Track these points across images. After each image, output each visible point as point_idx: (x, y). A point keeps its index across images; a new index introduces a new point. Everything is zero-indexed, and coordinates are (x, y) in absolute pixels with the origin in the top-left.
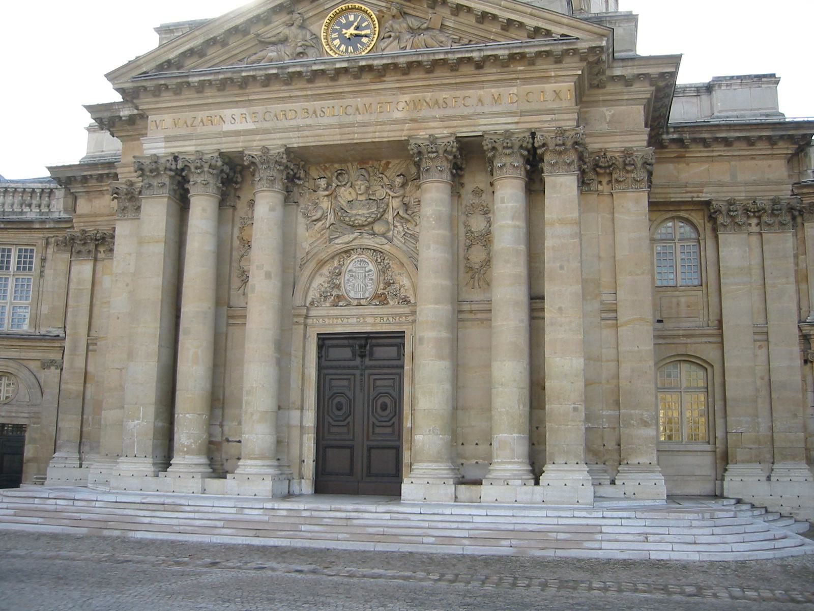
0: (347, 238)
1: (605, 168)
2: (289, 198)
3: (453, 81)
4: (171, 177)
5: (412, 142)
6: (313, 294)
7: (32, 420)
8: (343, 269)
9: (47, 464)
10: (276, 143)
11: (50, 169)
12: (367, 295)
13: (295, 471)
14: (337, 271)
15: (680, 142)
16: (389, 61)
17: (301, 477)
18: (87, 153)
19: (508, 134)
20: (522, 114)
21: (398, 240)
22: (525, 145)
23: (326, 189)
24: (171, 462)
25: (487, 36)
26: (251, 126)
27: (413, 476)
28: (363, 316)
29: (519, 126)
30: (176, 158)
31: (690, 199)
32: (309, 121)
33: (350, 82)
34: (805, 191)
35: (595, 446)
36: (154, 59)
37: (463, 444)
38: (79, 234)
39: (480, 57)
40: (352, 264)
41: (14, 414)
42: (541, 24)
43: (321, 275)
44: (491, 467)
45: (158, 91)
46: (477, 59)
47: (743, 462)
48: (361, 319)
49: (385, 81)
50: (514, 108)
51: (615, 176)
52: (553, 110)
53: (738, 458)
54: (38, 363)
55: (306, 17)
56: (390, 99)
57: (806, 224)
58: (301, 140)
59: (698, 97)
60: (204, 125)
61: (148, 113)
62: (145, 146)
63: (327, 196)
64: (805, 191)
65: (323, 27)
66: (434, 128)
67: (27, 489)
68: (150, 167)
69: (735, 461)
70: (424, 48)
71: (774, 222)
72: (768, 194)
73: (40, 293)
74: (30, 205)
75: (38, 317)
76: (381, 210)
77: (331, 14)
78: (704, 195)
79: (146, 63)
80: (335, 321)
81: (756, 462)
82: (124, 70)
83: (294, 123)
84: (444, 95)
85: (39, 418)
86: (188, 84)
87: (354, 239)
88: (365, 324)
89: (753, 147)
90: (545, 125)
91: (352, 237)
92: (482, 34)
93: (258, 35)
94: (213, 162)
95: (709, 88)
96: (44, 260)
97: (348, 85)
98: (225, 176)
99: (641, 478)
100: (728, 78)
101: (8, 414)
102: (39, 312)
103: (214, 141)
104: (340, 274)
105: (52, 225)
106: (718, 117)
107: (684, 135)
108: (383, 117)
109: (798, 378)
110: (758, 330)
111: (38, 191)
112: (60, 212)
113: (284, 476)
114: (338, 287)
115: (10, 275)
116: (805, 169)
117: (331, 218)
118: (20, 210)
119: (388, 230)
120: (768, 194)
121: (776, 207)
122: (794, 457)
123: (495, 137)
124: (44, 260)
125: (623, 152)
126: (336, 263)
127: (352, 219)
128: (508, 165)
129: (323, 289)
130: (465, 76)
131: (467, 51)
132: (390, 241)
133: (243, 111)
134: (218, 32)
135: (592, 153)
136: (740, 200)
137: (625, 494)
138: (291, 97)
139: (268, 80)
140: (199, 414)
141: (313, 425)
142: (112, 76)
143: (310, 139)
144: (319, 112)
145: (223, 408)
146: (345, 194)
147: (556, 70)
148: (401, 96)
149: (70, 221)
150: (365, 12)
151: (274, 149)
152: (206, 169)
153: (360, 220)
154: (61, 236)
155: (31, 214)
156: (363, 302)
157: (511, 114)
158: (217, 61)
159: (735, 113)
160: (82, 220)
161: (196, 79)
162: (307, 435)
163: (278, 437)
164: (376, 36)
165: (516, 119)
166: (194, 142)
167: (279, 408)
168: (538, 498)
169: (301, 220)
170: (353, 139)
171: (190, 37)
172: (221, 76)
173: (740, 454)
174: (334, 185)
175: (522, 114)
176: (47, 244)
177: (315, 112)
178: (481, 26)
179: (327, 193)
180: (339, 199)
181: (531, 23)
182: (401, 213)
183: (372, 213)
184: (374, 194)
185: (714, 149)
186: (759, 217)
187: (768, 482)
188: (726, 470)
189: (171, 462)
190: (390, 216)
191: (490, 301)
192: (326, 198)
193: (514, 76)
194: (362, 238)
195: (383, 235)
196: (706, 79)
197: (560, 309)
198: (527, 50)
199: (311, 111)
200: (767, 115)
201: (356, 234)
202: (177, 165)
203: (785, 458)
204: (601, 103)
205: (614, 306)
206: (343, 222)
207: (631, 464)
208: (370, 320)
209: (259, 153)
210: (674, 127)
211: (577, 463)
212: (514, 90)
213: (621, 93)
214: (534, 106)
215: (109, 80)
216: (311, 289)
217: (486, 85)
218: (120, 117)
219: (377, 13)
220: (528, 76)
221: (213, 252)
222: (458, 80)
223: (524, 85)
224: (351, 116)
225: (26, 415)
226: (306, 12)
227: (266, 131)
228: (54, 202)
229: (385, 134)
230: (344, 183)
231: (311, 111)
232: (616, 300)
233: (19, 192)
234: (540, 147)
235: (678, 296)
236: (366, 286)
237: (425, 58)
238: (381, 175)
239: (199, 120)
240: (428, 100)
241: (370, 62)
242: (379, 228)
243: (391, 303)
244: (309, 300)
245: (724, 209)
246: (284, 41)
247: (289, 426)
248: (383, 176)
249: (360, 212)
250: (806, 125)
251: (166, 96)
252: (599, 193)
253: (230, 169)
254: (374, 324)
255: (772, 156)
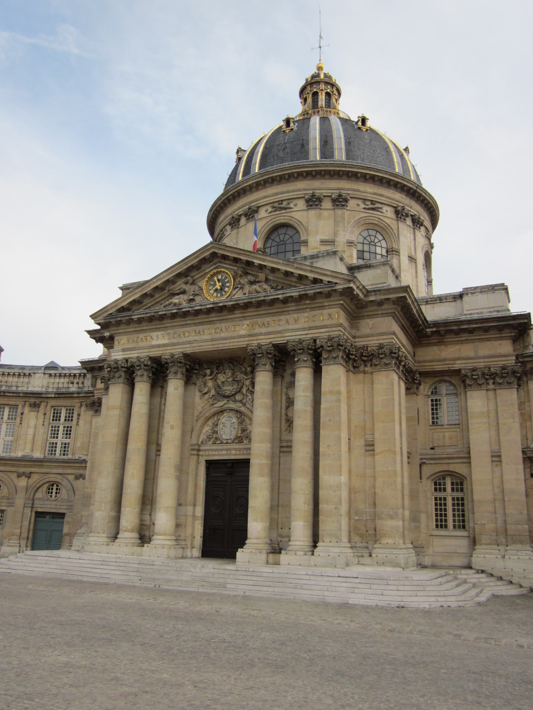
0: (221, 404)
1: (368, 357)
2: (188, 381)
3: (272, 311)
4: (125, 372)
5: (249, 348)
6: (203, 437)
7: (68, 510)
8: (220, 421)
9: (74, 536)
10: (178, 351)
11: (81, 362)
12: (232, 437)
13: (189, 543)
14: (216, 423)
15: (437, 333)
16: (235, 303)
17: (193, 547)
18: (103, 352)
19: (300, 342)
20: (310, 328)
21: (249, 404)
22: (310, 347)
23: (210, 375)
24: (118, 536)
25: (291, 283)
26: (166, 341)
27: (247, 547)
28: (230, 450)
29: (306, 336)
30: (127, 360)
31: (448, 369)
32: (197, 338)
33: (216, 315)
34: (527, 359)
35: (361, 531)
36: (115, 306)
37: (282, 528)
38: (97, 400)
39: (283, 297)
40: (224, 419)
41: (58, 507)
42: (316, 276)
43: (208, 425)
44: (291, 543)
45: (119, 323)
46: (281, 299)
47: (486, 544)
48: (229, 451)
49: (235, 313)
50: (306, 325)
51: (374, 361)
52: (326, 325)
53: (483, 542)
54: (73, 476)
55: (195, 278)
56: (238, 323)
57: (529, 382)
58: (191, 349)
59: (456, 302)
60: (142, 341)
61: (114, 335)
62: (112, 354)
63: (211, 379)
64: (527, 359)
65: (205, 283)
66: (261, 339)
67: (62, 553)
68: (114, 366)
69: (480, 543)
70: (255, 293)
71: (503, 382)
72: (499, 363)
73: (76, 434)
74: (73, 383)
75: (75, 448)
76: (239, 387)
77: (209, 276)
78: (457, 366)
79: (111, 308)
80: (215, 453)
81: (495, 544)
82: (100, 313)
83: (188, 339)
84: (268, 319)
85: (72, 509)
86: (132, 319)
87: (224, 404)
88: (230, 454)
89: (488, 333)
90: (322, 335)
91: (223, 403)
92: (288, 283)
93: (169, 290)
94: (146, 363)
95: (461, 296)
96: (79, 415)
97: (216, 317)
98: (154, 370)
99: (387, 552)
100: (473, 289)
101: (56, 507)
102: (75, 446)
103: (146, 350)
104: (217, 425)
105: (83, 395)
106: (465, 315)
107: (440, 328)
108: (235, 334)
109: (522, 488)
110: (495, 454)
111: (77, 375)
112: (89, 387)
113: (179, 546)
114: (217, 432)
115: (60, 424)
116: (528, 344)
117: (213, 392)
118: (67, 386)
119: (243, 399)
120: (499, 363)
121: (503, 371)
122: (521, 542)
123: (294, 344)
124: (79, 415)
125: (378, 346)
126: (216, 418)
127: (223, 392)
128: (301, 359)
129: (208, 434)
130: (278, 308)
131: (276, 295)
132: (244, 405)
133: (163, 333)
134: (148, 289)
135: (360, 348)
136: (480, 368)
137: (377, 563)
138: (187, 324)
139: (174, 316)
140: (133, 508)
141: (201, 515)
142: (94, 317)
143: (196, 348)
144: (201, 332)
145: (152, 505)
146: (221, 378)
147: (328, 302)
148: (245, 321)
149: (92, 393)
150: (227, 273)
151: (177, 354)
152: (142, 367)
153: (228, 393)
154: (89, 401)
155: (73, 388)
156: (229, 441)
157: (304, 329)
158: (149, 305)
159: (477, 311)
160: (99, 391)
161: (136, 317)
162: (197, 521)
163: (176, 522)
164: (232, 287)
165: (306, 332)
166: (136, 352)
167: (180, 505)
168: (312, 563)
169: (198, 394)
170: (219, 347)
171: (133, 293)
172: (148, 315)
173: (484, 539)
174: (215, 373)
175: (310, 328)
176: (81, 405)
177: (199, 332)
178: (287, 278)
179: (210, 377)
180: (218, 381)
181: (311, 276)
182: (250, 388)
183: (234, 389)
184: (236, 377)
185: (462, 336)
186: (494, 379)
187: (370, 557)
188: (474, 549)
189: (118, 536)
190: (244, 390)
191: (291, 441)
192: (210, 380)
193: (305, 306)
194: (228, 403)
195: (241, 401)
196: (457, 289)
197: (328, 446)
198: (308, 292)
199: (197, 332)
200: (498, 311)
201: (225, 401)
202: (127, 364)
203: (514, 542)
204: (366, 317)
205: (372, 442)
206: (219, 394)
207: (383, 544)
208: (233, 452)
209: (169, 357)
210: (433, 324)
211: (337, 542)
212: (306, 315)
213: (377, 310)
214: (317, 324)
215: (93, 319)
216: (202, 434)
217: (290, 312)
218: (104, 337)
219: (233, 273)
220: (313, 306)
221: (146, 414)
222: (275, 311)
223: (311, 311)
224: (218, 334)
225: (66, 507)
226: (195, 275)
227: (174, 345)
228: (86, 381)
229: (235, 344)
230: (220, 371)
231: (197, 332)
232: (374, 438)
233: (67, 376)
234: (319, 348)
235: (444, 432)
236: (231, 431)
237: (254, 300)
238: (240, 366)
239: (140, 339)
240: (259, 323)
241: (225, 304)
242: (238, 397)
243: (245, 442)
244: (201, 440)
245: (469, 374)
246: (184, 292)
247: (186, 515)
248: (242, 366)
249: (228, 388)
250: (520, 317)
251: (122, 326)
252: (365, 372)
253: (157, 365)
254: (235, 455)
255: (501, 338)
